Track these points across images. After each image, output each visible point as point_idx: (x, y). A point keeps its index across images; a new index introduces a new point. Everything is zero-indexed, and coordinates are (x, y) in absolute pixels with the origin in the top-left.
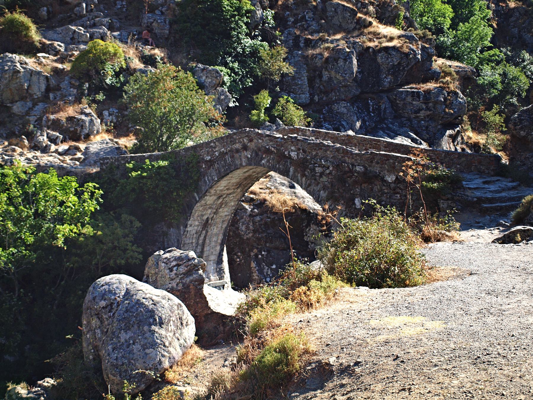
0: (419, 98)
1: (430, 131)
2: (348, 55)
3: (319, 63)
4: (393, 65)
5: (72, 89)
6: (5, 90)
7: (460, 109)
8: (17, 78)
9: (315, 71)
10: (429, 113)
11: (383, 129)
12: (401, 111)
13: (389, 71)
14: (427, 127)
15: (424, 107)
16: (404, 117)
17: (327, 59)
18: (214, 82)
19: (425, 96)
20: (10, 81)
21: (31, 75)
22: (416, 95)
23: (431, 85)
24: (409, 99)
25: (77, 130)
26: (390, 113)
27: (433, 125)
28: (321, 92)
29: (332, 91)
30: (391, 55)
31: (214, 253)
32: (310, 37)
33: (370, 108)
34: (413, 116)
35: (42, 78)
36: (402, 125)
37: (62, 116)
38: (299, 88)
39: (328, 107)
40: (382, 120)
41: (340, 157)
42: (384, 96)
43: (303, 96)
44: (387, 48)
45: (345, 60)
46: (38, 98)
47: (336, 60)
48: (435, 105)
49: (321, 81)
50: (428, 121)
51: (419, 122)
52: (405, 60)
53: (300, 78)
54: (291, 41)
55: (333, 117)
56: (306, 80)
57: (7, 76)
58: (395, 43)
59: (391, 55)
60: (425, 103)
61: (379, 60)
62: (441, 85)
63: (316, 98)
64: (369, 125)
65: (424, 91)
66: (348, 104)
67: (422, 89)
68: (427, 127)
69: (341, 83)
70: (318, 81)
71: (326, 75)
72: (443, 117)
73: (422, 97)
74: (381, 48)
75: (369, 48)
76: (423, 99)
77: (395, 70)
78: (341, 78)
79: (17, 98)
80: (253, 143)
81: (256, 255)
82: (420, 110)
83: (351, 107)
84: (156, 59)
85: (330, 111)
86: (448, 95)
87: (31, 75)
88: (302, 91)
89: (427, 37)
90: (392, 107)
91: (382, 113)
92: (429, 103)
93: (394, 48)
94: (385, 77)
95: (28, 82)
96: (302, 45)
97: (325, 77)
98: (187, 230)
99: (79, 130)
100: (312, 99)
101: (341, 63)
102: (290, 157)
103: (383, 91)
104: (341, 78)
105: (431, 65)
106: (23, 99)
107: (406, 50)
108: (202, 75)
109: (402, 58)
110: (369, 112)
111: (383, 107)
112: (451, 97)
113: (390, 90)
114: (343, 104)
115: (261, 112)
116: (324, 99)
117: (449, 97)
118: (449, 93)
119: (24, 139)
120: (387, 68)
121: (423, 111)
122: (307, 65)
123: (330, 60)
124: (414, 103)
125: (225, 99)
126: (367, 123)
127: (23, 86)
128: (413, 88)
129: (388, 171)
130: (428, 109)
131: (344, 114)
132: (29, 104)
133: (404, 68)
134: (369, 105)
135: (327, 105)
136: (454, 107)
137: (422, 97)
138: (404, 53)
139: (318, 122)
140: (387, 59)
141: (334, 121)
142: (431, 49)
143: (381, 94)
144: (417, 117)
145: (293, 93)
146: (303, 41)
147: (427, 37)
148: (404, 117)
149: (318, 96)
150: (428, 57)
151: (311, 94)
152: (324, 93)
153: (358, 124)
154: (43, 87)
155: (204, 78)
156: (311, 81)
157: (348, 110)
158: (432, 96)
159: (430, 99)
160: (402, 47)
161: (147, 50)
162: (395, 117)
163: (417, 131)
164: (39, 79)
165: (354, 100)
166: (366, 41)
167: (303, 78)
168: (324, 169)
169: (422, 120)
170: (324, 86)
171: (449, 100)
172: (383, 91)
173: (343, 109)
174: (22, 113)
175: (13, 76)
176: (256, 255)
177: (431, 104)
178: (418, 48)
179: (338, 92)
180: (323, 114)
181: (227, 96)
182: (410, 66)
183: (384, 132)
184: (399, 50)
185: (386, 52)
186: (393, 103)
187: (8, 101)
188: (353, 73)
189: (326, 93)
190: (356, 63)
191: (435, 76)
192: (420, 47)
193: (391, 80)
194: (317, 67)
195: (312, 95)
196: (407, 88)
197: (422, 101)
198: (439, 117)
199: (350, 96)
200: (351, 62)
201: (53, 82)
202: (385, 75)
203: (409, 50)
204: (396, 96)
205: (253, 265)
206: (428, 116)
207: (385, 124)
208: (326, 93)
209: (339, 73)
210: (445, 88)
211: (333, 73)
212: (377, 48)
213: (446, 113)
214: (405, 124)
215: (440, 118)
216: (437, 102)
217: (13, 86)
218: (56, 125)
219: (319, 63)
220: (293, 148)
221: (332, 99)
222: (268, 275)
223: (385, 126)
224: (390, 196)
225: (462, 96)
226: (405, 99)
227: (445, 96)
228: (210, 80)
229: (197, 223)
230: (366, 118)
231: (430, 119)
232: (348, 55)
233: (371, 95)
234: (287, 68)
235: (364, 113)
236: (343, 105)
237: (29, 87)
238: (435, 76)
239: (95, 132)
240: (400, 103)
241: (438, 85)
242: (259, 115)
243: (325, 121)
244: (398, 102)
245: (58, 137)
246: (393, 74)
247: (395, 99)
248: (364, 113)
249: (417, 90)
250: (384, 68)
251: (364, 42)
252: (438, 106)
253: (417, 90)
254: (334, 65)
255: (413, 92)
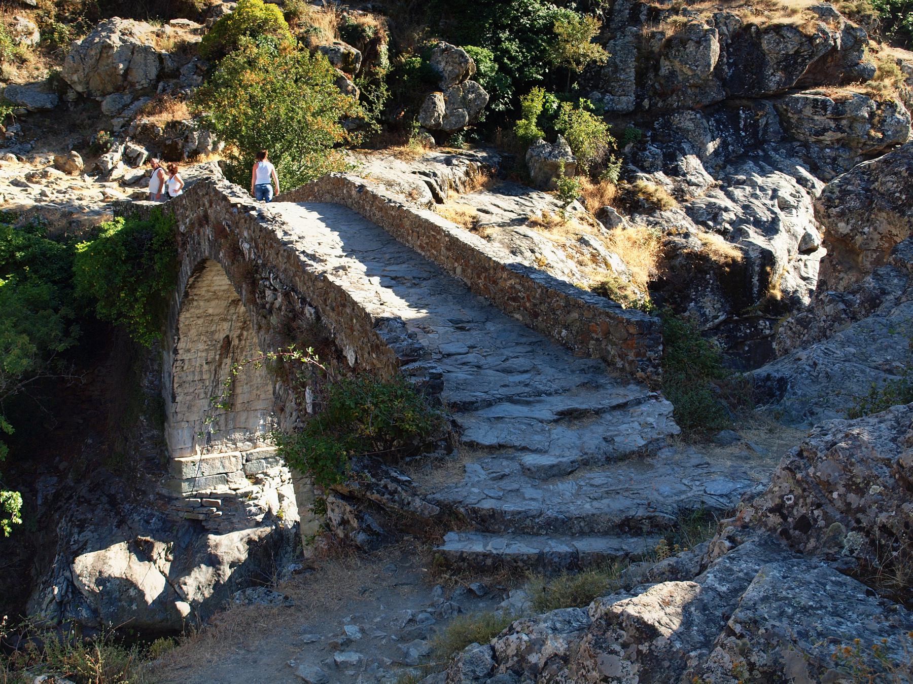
0: (826, 111)
1: (838, 165)
2: (705, 36)
3: (656, 46)
4: (787, 54)
5: (195, 77)
6: (91, 74)
7: (897, 132)
8: (108, 57)
9: (647, 59)
10: (839, 135)
11: (756, 159)
12: (794, 131)
13: (778, 63)
14: (834, 159)
15: (833, 126)
16: (799, 141)
17: (670, 40)
18: (457, 71)
19: (835, 108)
20: (98, 61)
21: (133, 53)
22: (820, 106)
23: (851, 91)
24: (808, 111)
25: (177, 144)
26: (774, 132)
27: (846, 155)
28: (656, 93)
29: (672, 93)
30: (784, 38)
31: (263, 396)
32: (657, 5)
33: (739, 123)
34: (812, 139)
35: (151, 58)
36: (791, 154)
37: (160, 120)
38: (620, 86)
39: (663, 118)
40: (759, 143)
42: (769, 105)
43: (624, 99)
44: (778, 28)
45: (699, 43)
46: (143, 89)
47: (683, 42)
48: (852, 123)
49: (656, 75)
50: (838, 149)
51: (822, 149)
52: (806, 47)
53: (624, 70)
54: (627, 11)
55: (670, 135)
56: (633, 74)
57: (93, 53)
58: (797, 20)
59: (784, 38)
60: (835, 120)
61: (765, 46)
62: (869, 90)
63: (646, 103)
64: (733, 151)
65: (835, 100)
66: (698, 115)
67: (833, 96)
68: (834, 159)
69: (688, 81)
70: (652, 76)
71: (665, 67)
72: (865, 144)
73: (830, 108)
74: (769, 26)
75: (751, 25)
76: (832, 113)
77: (789, 63)
78: (690, 73)
79: (110, 88)
82: (825, 130)
83: (704, 121)
84: (364, 31)
85: (667, 125)
86: (878, 108)
87: (133, 53)
88: (623, 91)
89: (863, 13)
90: (781, 123)
91: (761, 133)
92: (842, 119)
93: (791, 27)
94: (772, 74)
95: (127, 63)
96: (643, 17)
97: (664, 71)
98: (179, 357)
99: (180, 144)
100: (639, 105)
101: (691, 47)
103: (768, 97)
104: (690, 73)
105: (860, 58)
106: (119, 89)
107: (811, 31)
108: (440, 59)
109: (801, 44)
110: (737, 130)
111: (762, 122)
112: (883, 111)
113: (779, 95)
114: (689, 115)
115: (530, 123)
116: (659, 105)
117: (880, 112)
118: (879, 105)
119: (75, 156)
120: (776, 58)
121: (830, 133)
122: (639, 49)
123: (674, 42)
124: (816, 118)
125: (475, 99)
126: (730, 148)
127: (116, 68)
128: (819, 94)
130: (839, 129)
131: (688, 131)
132: (127, 98)
133: (804, 61)
134: (739, 117)
135: (663, 116)
136: (886, 128)
137: (830, 108)
138: (806, 36)
139: (639, 142)
140: (778, 44)
141: (670, 142)
142: (861, 30)
143: (764, 102)
144: (820, 141)
145: (611, 93)
146: (645, 12)
147: (863, 13)
148: (799, 141)
149: (650, 100)
150: (854, 42)
151: (637, 97)
152: (660, 96)
153: (711, 147)
154: (153, 72)
155: (443, 64)
156: (641, 76)
157: (696, 126)
158: (847, 109)
159: (843, 112)
160: (804, 26)
161: (355, 18)
162: (784, 140)
163: (816, 164)
164: (145, 59)
165: (709, 110)
166: (749, 14)
167: (628, 70)
169: (827, 146)
170: (660, 84)
171: (879, 116)
172: (768, 97)
173: (687, 123)
174: (112, 112)
175: (101, 53)
177: (844, 122)
178: (837, 28)
179: (683, 94)
180: (654, 129)
181: (481, 95)
182: (816, 58)
183: (756, 164)
184: (799, 31)
185: (777, 33)
186: (782, 117)
187: (98, 93)
188: (710, 65)
189: (663, 96)
190: (718, 50)
191: (864, 76)
192: (843, 27)
193: (781, 79)
194: (652, 52)
195: (639, 98)
196: (809, 94)
197: (829, 116)
198: (858, 143)
199: (706, 102)
200: (708, 48)
201: (169, 64)
202: (772, 71)
203: (818, 30)
204: (787, 105)
206: (838, 141)
207: (764, 150)
208: (663, 96)
209: (687, 63)
210: (874, 95)
211: (677, 63)
212: (764, 26)
213: (871, 138)
214: (797, 153)
215: (860, 145)
216: (854, 119)
217: (102, 68)
218: (146, 135)
219: (656, 46)
221: (672, 105)
223: (761, 153)
225: (904, 110)
226: (801, 111)
227: (871, 109)
228: (450, 68)
229: (201, 346)
230: (729, 139)
231: (843, 146)
232: (705, 36)
233: (745, 102)
234: (598, 53)
235: (729, 131)
236: (689, 117)
237: (127, 71)
238: (864, 76)
239: (210, 148)
240: (794, 118)
241: (864, 91)
242: (526, 127)
243: (654, 141)
244: (790, 115)
245: (140, 155)
246: (784, 70)
247: (786, 110)
248: (729, 131)
249: (823, 97)
250: (771, 59)
251: (745, 16)
252: (858, 126)
253: (823, 97)
254: (679, 51)
255: (816, 100)
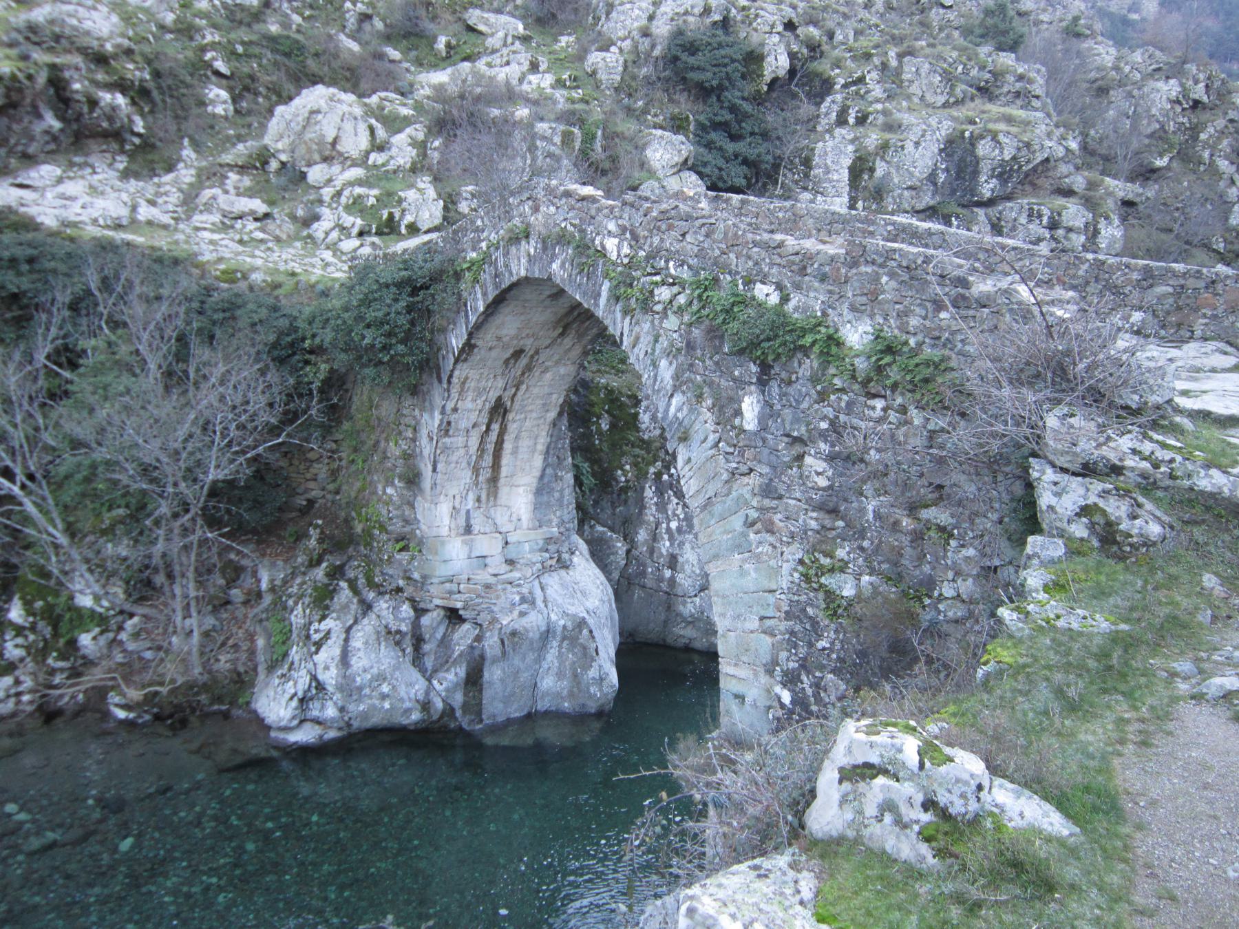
41: (717, 252)
42: (980, 212)
80: (540, 217)
81: (658, 475)
97: (879, 173)
102: (603, 253)
103: (980, 204)
109: (1019, 149)
129: (853, 308)
168: (676, 289)
176: (658, 475)
205: (649, 492)
217: (309, 135)
220: (612, 226)
222: (675, 514)
224: (849, 404)
246: (1000, 176)
